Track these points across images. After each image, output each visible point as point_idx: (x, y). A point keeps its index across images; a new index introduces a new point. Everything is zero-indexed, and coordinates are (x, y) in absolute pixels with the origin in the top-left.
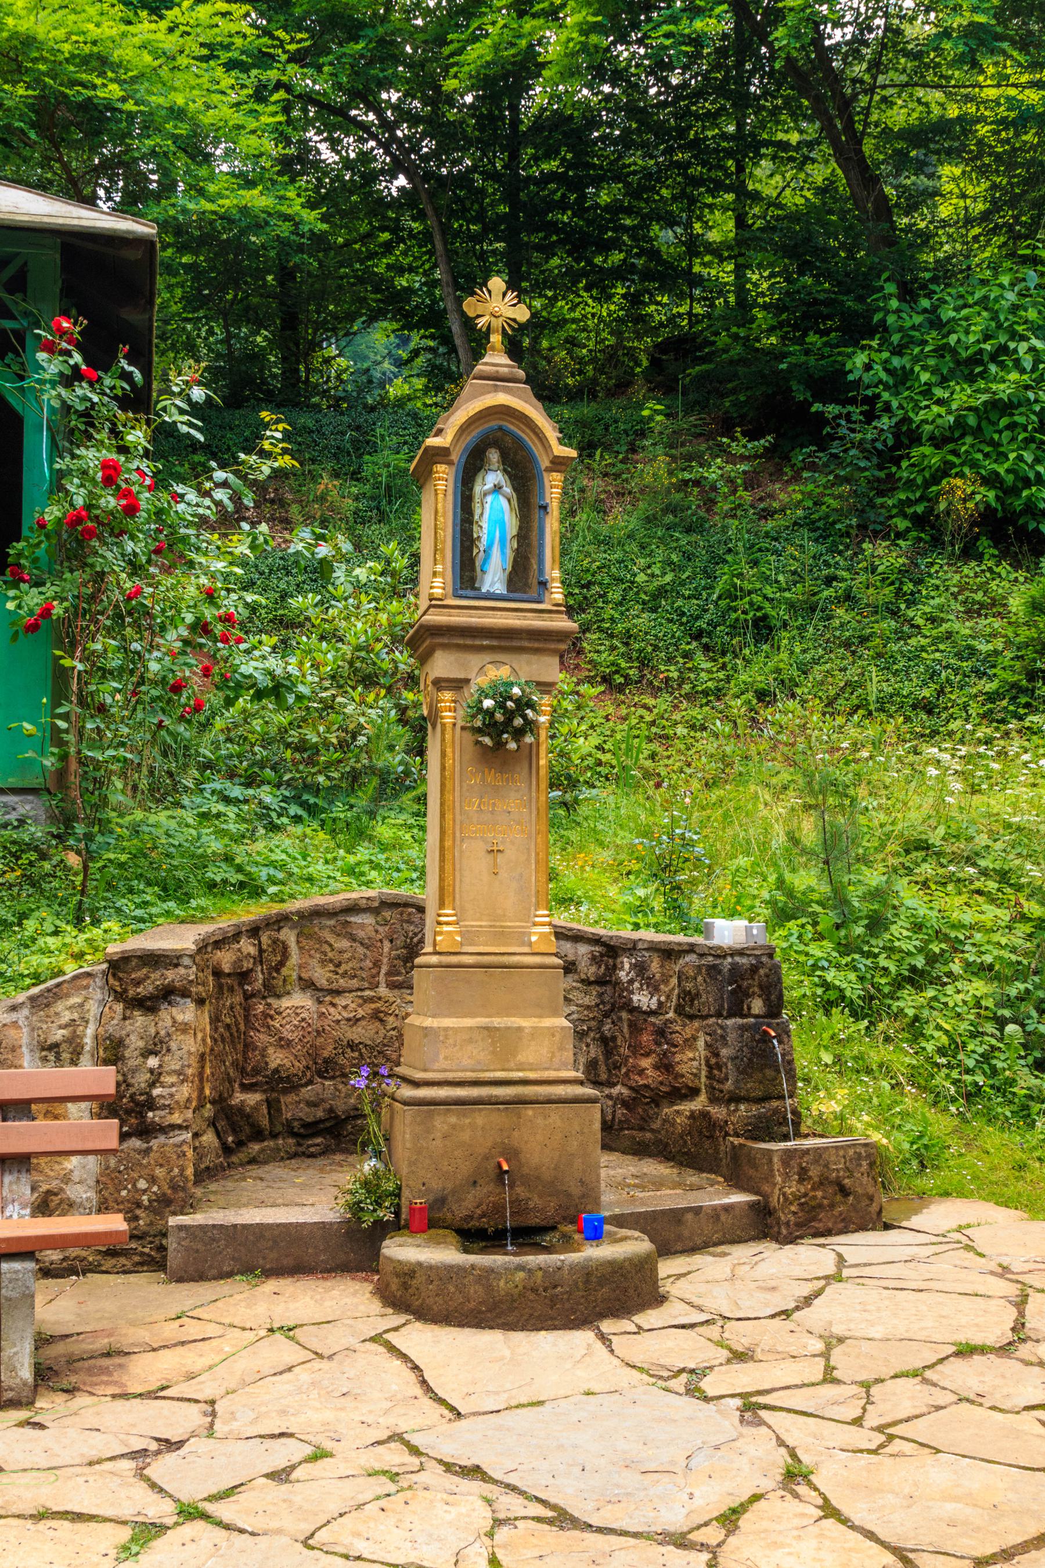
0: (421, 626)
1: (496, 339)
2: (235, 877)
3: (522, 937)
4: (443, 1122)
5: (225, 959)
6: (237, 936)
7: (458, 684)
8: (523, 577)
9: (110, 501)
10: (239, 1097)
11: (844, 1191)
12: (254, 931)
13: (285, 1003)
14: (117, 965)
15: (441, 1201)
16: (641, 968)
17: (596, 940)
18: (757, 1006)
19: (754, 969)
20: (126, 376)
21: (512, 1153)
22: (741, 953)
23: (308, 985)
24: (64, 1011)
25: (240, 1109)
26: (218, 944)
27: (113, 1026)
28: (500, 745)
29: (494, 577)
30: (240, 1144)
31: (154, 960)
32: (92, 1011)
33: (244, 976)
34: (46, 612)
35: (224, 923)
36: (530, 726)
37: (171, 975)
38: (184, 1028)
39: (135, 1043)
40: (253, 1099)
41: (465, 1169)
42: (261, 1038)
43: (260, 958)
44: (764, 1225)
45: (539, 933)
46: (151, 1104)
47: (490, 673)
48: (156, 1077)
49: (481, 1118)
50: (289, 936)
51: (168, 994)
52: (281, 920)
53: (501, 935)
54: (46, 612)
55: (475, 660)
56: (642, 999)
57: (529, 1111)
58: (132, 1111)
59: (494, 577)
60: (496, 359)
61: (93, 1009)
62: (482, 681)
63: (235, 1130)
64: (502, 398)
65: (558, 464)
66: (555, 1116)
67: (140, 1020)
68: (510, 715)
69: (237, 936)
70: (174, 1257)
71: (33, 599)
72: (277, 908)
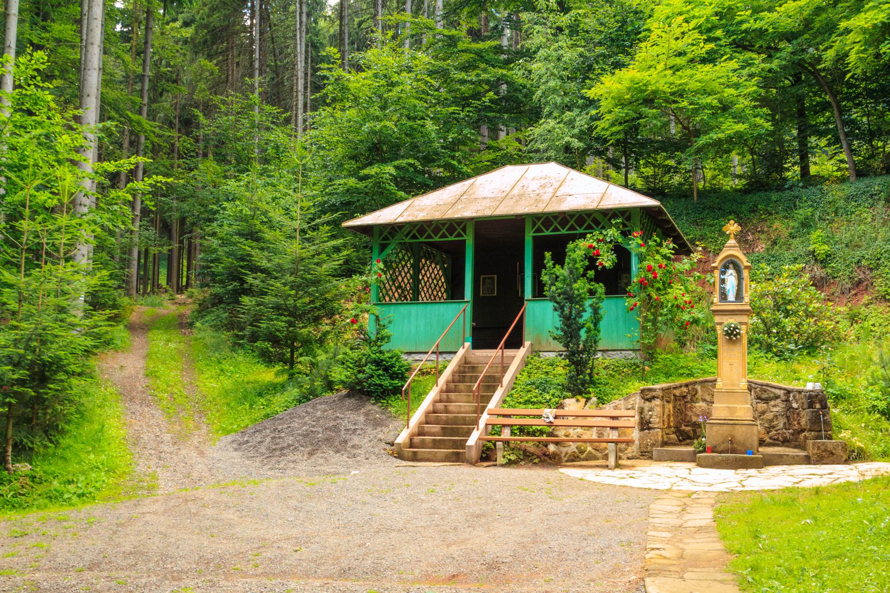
0: (496, 348)
1: (732, 236)
2: (688, 372)
3: (738, 385)
4: (715, 428)
5: (677, 392)
6: (681, 387)
7: (721, 324)
8: (739, 297)
9: (650, 276)
10: (683, 428)
11: (832, 454)
12: (687, 385)
13: (697, 405)
14: (643, 391)
15: (715, 447)
16: (794, 396)
17: (785, 389)
18: (818, 406)
19: (817, 396)
20: (656, 241)
21: (733, 436)
22: (812, 391)
23: (704, 400)
24: (631, 401)
25: (684, 431)
26: (674, 388)
27: (642, 405)
28: (731, 339)
29: (731, 297)
30: (684, 440)
31: (650, 390)
32: (637, 401)
33: (684, 397)
34: (635, 305)
35: (677, 383)
36: (739, 334)
37: (654, 394)
38: (657, 406)
39: (646, 409)
40: (688, 429)
41: (721, 439)
42: (689, 413)
43: (689, 392)
44: (807, 460)
45: (744, 385)
46: (650, 422)
47: (732, 321)
48: (651, 416)
49: (725, 428)
50: (698, 387)
51: (654, 398)
52: (695, 383)
53: (733, 385)
54: (635, 305)
55: (725, 318)
56: (795, 405)
57: (737, 427)
58: (645, 425)
59: (731, 297)
60: (732, 242)
61: (637, 401)
62: (726, 323)
63: (682, 435)
64: (731, 252)
65: (746, 267)
66: (744, 428)
67: (647, 403)
68: (732, 332)
69: (681, 387)
70: (654, 456)
71: (633, 301)
72: (694, 380)
